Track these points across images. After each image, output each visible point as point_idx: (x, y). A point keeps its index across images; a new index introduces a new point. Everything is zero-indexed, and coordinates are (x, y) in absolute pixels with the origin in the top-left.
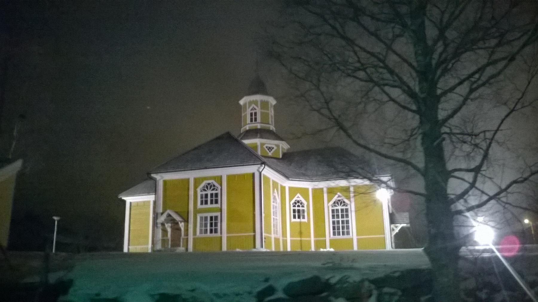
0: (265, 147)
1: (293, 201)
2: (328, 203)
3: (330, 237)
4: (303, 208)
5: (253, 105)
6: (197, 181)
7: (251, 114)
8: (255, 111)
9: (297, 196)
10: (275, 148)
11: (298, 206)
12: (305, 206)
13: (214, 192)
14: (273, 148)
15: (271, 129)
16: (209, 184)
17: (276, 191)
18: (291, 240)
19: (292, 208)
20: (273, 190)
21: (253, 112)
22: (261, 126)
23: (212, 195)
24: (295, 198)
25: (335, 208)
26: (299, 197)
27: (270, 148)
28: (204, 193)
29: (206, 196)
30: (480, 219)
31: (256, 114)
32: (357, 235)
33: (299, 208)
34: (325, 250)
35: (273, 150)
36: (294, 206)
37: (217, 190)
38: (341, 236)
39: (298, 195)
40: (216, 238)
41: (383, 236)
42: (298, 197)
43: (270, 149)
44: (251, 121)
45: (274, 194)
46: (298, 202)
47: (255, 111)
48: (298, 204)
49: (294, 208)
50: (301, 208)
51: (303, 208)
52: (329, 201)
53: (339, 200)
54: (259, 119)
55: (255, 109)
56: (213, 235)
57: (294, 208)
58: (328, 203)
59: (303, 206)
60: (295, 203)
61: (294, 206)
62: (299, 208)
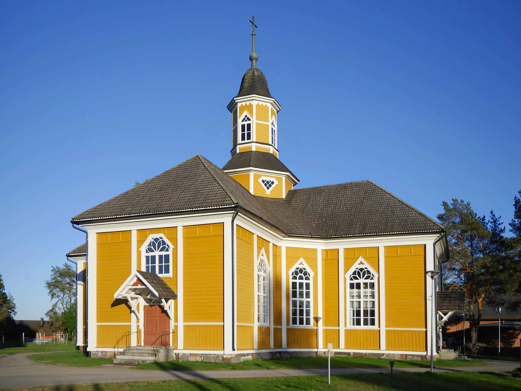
0: (260, 180)
1: (293, 269)
2: (345, 272)
3: (346, 326)
4: (307, 281)
5: (245, 113)
6: (143, 233)
7: (243, 126)
8: (248, 122)
9: (299, 262)
10: (276, 182)
11: (301, 278)
12: (311, 278)
13: (163, 253)
14: (273, 183)
15: (271, 152)
16: (156, 240)
17: (263, 251)
18: (387, 331)
19: (291, 281)
20: (259, 249)
21: (246, 123)
22: (256, 148)
23: (161, 257)
24: (297, 265)
25: (355, 281)
26: (301, 263)
27: (268, 182)
28: (150, 254)
29: (153, 258)
30: (62, 268)
31: (249, 126)
32: (387, 326)
33: (301, 281)
34: (220, 352)
35: (273, 186)
36: (295, 278)
37: (167, 250)
38: (362, 327)
39: (302, 260)
40: (373, 331)
41: (338, 328)
42: (301, 263)
43: (268, 184)
44: (243, 139)
45: (261, 257)
46: (301, 271)
47: (248, 122)
48: (300, 274)
49: (294, 281)
50: (304, 281)
51: (307, 281)
52: (346, 271)
53: (361, 269)
54: (254, 138)
55: (249, 120)
56: (369, 327)
57: (294, 281)
58: (345, 272)
59: (307, 279)
60: (296, 273)
61: (295, 278)
62: (301, 281)
